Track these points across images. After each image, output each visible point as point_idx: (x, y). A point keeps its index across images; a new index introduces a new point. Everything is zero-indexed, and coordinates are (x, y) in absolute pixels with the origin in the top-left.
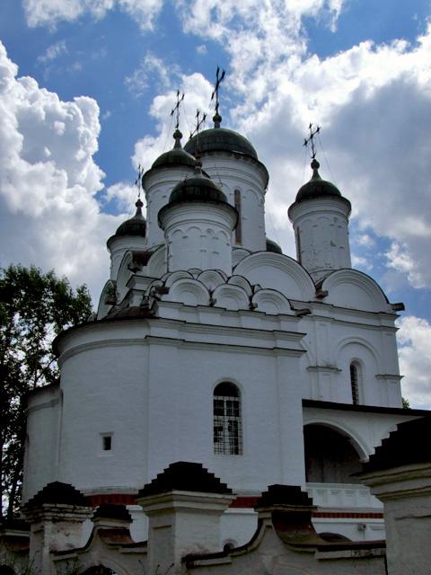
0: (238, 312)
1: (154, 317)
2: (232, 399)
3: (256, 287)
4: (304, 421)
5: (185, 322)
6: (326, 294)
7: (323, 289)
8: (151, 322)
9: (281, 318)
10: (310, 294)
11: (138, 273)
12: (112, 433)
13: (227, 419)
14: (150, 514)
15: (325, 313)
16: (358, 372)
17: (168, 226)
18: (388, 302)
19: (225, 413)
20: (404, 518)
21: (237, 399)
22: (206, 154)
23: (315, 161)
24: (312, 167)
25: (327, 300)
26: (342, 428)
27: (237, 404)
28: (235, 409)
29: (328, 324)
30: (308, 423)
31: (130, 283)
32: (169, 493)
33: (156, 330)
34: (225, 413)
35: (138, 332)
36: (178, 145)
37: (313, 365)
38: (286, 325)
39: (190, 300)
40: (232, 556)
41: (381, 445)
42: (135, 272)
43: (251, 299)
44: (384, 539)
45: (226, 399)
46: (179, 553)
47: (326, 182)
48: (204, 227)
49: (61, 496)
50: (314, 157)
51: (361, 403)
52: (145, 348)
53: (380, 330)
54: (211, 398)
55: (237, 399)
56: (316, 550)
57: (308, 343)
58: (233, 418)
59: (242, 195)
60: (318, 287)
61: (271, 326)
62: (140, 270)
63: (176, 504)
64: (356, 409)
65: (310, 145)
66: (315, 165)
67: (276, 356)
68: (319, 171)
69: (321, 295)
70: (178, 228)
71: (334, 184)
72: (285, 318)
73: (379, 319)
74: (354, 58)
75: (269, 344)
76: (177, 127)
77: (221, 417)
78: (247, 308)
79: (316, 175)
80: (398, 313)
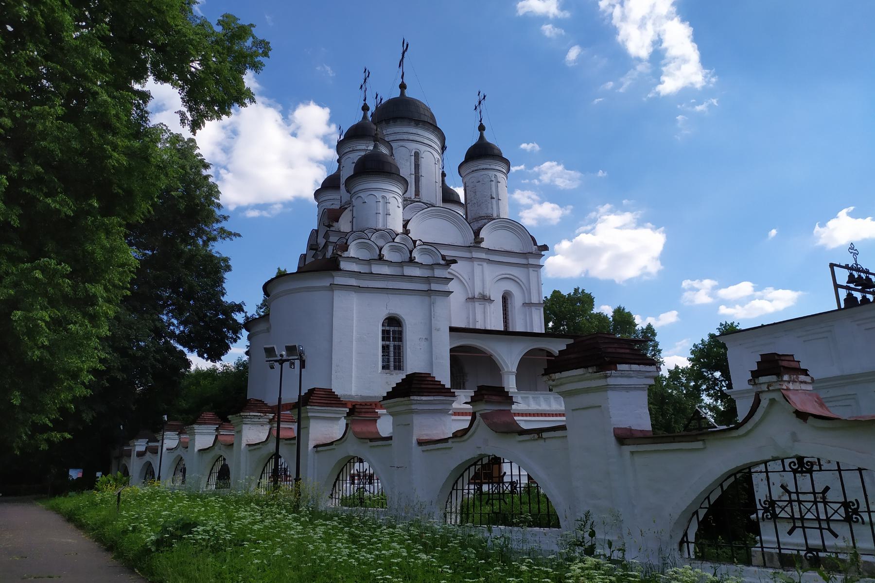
2: (396, 329)
3: (418, 242)
4: (450, 345)
5: (360, 272)
6: (482, 240)
7: (481, 236)
8: (334, 273)
11: (332, 229)
14: (391, 414)
15: (483, 256)
16: (509, 301)
17: (345, 151)
18: (535, 243)
19: (391, 340)
20: (577, 409)
22: (384, 123)
23: (481, 124)
24: (479, 130)
25: (483, 245)
26: (487, 349)
27: (401, 333)
28: (399, 337)
29: (485, 264)
30: (451, 347)
31: (326, 236)
32: (192, 426)
33: (339, 280)
34: (391, 340)
35: (326, 282)
36: (365, 117)
37: (470, 296)
38: (439, 273)
39: (364, 255)
40: (336, 445)
41: (401, 381)
42: (329, 228)
43: (411, 252)
45: (392, 329)
46: (196, 450)
47: (489, 144)
49: (329, 399)
50: (481, 121)
51: (511, 330)
53: (527, 268)
54: (380, 328)
56: (368, 441)
57: (468, 280)
58: (396, 343)
61: (426, 273)
62: (333, 226)
63: (310, 414)
64: (506, 333)
65: (478, 110)
67: (430, 297)
68: (485, 133)
69: (478, 240)
70: (359, 195)
72: (437, 267)
73: (527, 259)
75: (424, 287)
76: (365, 100)
77: (387, 343)
79: (482, 137)
80: (543, 253)
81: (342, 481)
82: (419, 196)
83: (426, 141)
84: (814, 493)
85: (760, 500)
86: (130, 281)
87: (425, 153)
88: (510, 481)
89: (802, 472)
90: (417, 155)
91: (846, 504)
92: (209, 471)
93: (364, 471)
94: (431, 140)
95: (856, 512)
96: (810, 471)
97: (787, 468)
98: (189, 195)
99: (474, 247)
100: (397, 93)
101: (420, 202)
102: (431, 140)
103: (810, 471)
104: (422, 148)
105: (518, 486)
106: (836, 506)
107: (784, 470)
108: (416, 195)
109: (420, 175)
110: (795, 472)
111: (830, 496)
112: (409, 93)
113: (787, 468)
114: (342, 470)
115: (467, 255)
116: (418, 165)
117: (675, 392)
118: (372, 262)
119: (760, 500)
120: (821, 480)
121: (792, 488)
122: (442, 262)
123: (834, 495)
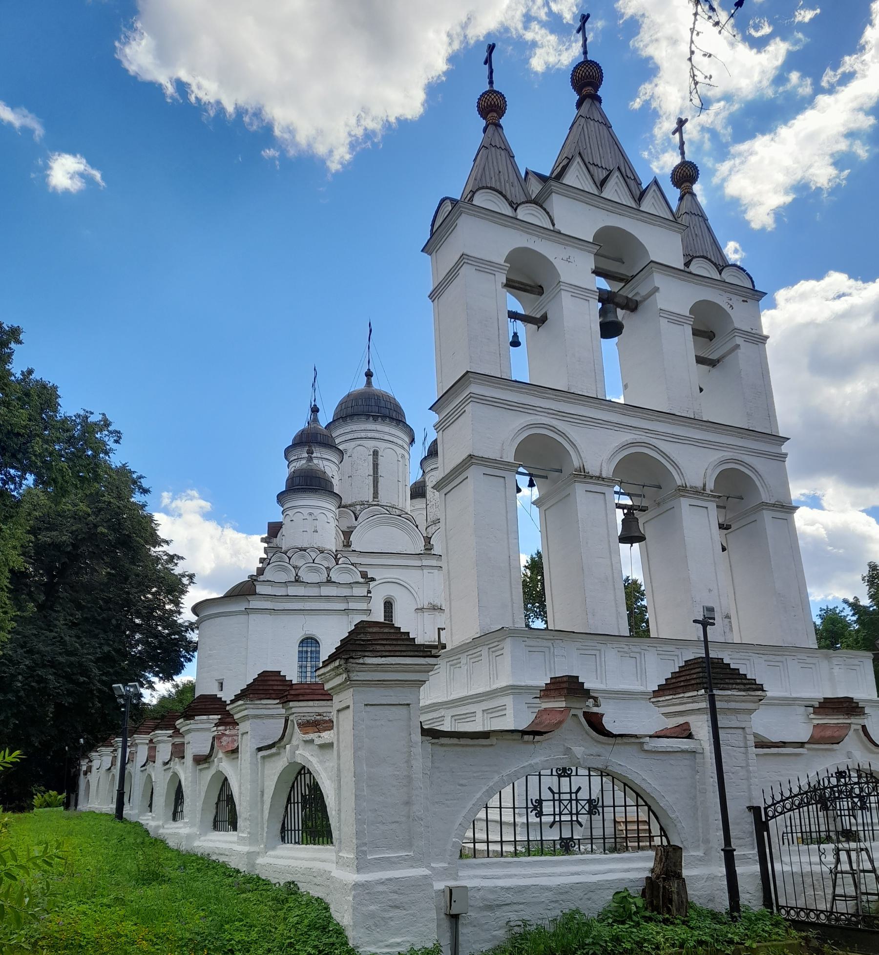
0: (319, 584)
1: (254, 593)
8: (249, 598)
9: (423, 568)
10: (420, 547)
12: (223, 679)
13: (309, 664)
21: (318, 649)
33: (255, 603)
39: (282, 577)
44: (620, 544)
48: (305, 511)
52: (246, 617)
54: (296, 649)
55: (318, 649)
57: (417, 589)
59: (380, 454)
60: (428, 540)
61: (346, 592)
63: (137, 741)
66: (369, 374)
71: (390, 393)
74: (725, 762)
75: (342, 606)
78: (293, 579)
81: (812, 830)
82: (377, 498)
83: (387, 437)
84: (571, 793)
85: (532, 800)
86: (171, 494)
87: (386, 451)
88: (588, 798)
89: (564, 776)
90: (375, 453)
91: (590, 801)
92: (217, 796)
93: (574, 790)
94: (398, 437)
95: (596, 807)
96: (569, 776)
97: (554, 773)
98: (117, 527)
99: (424, 554)
100: (360, 384)
101: (378, 505)
102: (398, 437)
103: (569, 776)
104: (381, 445)
105: (600, 803)
106: (583, 803)
107: (552, 775)
108: (374, 498)
109: (379, 474)
110: (559, 776)
111: (580, 795)
112: (378, 384)
113: (554, 773)
114: (293, 786)
115: (418, 563)
116: (377, 464)
117: (49, 757)
118: (289, 584)
119: (532, 800)
120: (576, 782)
121: (556, 790)
122: (362, 580)
123: (583, 795)
